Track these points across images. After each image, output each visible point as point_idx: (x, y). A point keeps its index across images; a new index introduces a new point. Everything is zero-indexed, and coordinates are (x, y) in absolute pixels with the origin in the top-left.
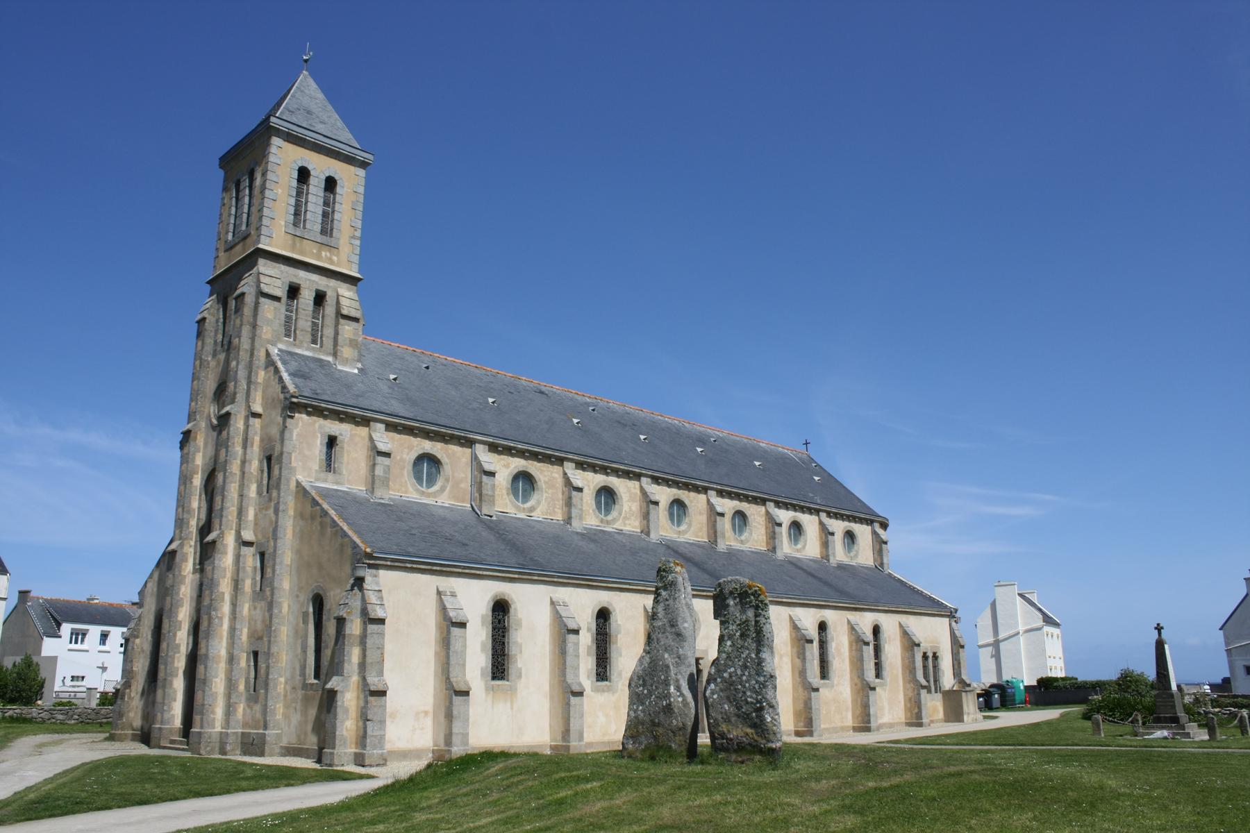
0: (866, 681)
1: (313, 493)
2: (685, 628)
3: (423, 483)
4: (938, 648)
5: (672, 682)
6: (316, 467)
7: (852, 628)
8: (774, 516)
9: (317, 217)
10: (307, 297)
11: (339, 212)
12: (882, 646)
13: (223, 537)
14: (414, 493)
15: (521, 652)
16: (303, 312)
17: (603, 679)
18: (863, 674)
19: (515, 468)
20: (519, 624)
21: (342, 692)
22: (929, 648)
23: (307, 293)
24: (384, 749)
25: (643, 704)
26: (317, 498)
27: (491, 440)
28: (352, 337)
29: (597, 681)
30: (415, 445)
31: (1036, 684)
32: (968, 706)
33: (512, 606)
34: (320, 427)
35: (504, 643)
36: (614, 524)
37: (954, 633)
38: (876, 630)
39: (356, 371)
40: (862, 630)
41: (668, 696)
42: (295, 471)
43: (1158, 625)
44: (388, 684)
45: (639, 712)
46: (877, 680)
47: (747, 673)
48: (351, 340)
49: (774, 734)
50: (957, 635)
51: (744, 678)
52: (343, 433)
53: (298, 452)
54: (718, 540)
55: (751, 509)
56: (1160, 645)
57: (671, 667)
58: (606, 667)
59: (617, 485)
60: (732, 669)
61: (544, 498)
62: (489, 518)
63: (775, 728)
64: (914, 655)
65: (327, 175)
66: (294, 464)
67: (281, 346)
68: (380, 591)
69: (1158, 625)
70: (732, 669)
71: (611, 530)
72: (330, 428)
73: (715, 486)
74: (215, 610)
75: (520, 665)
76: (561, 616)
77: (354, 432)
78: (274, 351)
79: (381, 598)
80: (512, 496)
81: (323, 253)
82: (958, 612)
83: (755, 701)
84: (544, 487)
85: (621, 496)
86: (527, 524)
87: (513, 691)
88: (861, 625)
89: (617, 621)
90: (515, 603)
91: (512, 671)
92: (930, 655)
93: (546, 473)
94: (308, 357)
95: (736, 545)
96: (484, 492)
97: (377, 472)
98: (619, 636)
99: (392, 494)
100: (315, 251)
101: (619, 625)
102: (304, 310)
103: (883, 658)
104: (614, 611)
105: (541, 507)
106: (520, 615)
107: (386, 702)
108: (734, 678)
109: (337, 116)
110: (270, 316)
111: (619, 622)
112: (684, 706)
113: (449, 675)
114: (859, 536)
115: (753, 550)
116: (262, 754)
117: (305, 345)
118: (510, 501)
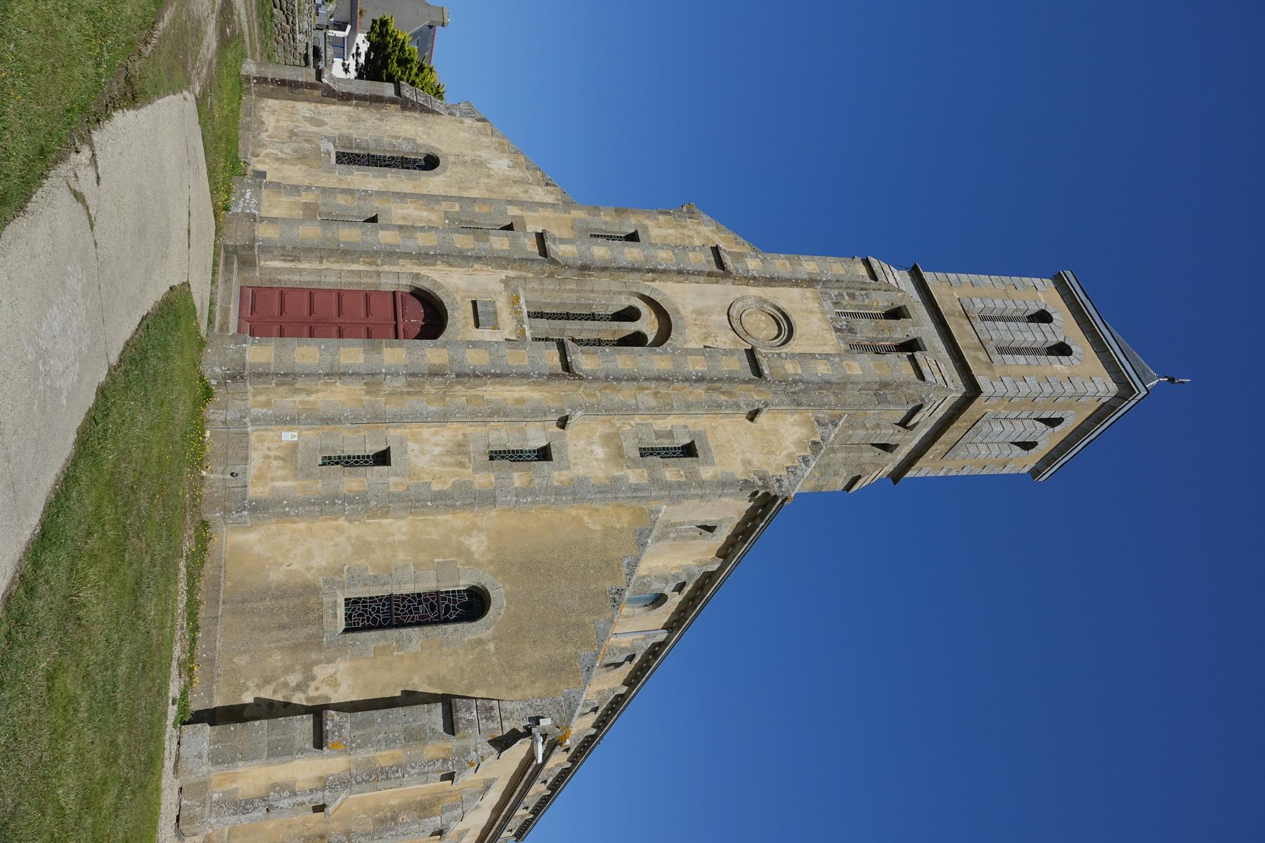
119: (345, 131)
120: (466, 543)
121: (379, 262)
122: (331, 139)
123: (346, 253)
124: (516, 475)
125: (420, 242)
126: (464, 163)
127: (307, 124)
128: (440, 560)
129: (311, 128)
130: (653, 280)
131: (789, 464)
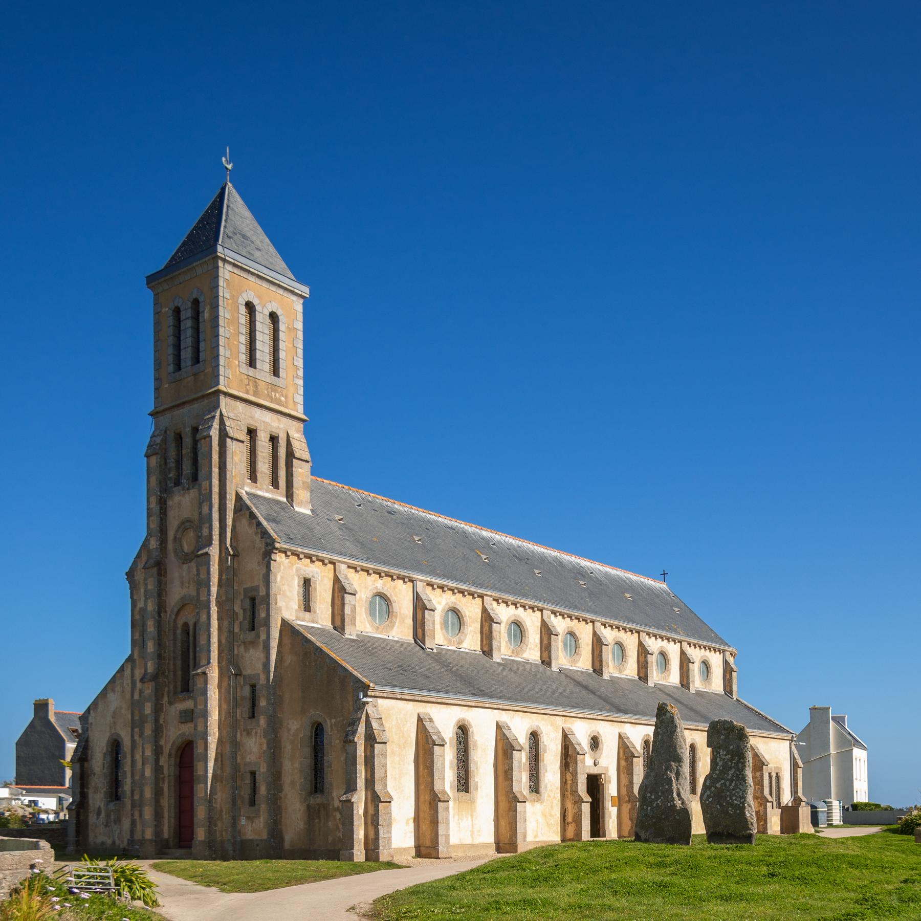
4: (779, 768)
6: (296, 606)
7: (622, 740)
9: (266, 356)
16: (261, 454)
20: (476, 745)
27: (429, 579)
33: (470, 730)
34: (298, 570)
39: (309, 513)
42: (281, 610)
47: (733, 784)
51: (731, 787)
52: (315, 575)
54: (603, 669)
60: (723, 781)
65: (270, 311)
67: (247, 489)
68: (381, 718)
71: (519, 659)
72: (305, 571)
89: (543, 742)
92: (774, 775)
101: (546, 745)
102: (262, 452)
106: (476, 738)
109: (269, 242)
115: (629, 677)
116: (599, 837)
117: (265, 487)
119: (102, 796)
120: (293, 731)
121: (162, 776)
122: (107, 804)
123: (158, 793)
124: (261, 704)
125: (149, 754)
126: (115, 723)
127: (101, 817)
128: (299, 745)
129: (103, 815)
130: (166, 612)
131: (259, 536)
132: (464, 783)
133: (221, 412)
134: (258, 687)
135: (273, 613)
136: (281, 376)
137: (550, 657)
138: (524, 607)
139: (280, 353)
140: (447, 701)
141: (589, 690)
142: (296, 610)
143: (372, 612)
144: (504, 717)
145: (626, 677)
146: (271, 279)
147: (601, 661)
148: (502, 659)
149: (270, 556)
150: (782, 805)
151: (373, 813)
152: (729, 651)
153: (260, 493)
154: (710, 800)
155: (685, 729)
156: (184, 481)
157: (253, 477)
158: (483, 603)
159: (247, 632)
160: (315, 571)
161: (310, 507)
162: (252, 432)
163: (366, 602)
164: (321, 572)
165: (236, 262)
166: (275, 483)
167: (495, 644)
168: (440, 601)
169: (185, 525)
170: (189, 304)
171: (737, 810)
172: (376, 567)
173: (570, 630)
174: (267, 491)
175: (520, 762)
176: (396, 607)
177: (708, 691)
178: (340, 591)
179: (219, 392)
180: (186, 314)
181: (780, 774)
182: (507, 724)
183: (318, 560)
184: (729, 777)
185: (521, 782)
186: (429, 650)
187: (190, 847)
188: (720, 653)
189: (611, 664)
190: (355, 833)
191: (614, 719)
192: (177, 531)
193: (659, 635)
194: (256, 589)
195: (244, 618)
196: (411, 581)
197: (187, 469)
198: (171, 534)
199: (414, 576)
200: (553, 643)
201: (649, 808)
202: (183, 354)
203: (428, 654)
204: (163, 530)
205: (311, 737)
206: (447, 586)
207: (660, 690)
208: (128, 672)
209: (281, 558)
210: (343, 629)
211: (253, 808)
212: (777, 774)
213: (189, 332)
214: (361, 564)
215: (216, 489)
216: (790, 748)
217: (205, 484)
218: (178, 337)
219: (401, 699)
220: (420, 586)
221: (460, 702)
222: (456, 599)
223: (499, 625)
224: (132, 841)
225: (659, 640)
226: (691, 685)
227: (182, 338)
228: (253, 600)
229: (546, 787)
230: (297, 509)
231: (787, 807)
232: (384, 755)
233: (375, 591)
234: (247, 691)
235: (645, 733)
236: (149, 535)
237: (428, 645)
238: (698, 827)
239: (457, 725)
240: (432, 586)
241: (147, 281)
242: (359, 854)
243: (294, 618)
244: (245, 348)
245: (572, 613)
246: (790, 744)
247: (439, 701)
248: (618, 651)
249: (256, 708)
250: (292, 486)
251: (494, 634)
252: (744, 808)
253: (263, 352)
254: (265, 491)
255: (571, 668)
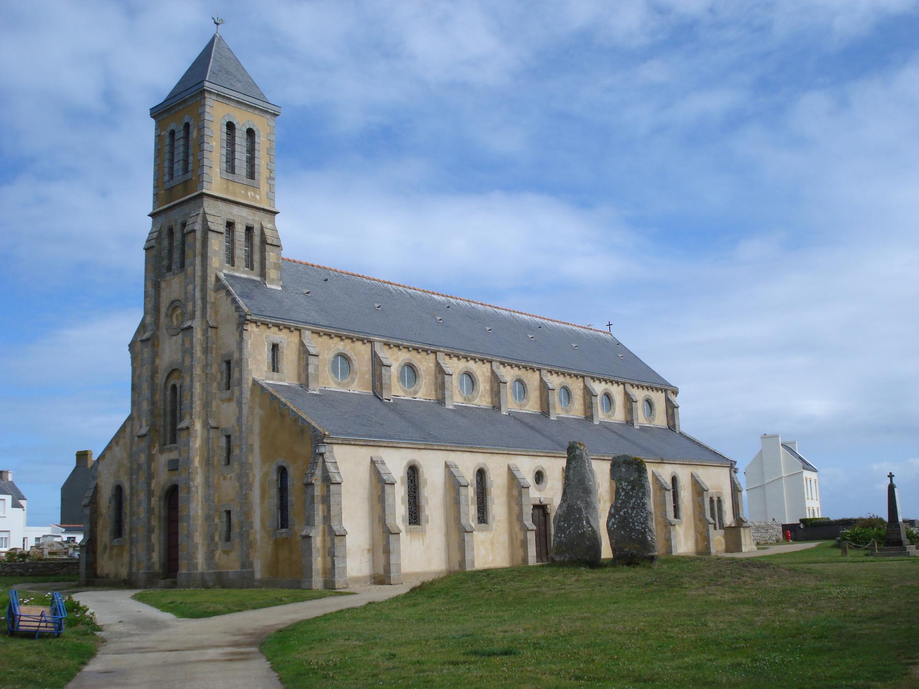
0: (668, 519)
1: (270, 389)
2: (590, 485)
3: (338, 376)
4: (721, 493)
5: (584, 519)
6: (265, 368)
8: (591, 390)
10: (240, 230)
11: (259, 158)
12: (679, 493)
13: (194, 424)
14: (334, 384)
15: (427, 503)
17: (481, 522)
18: (666, 515)
19: (402, 360)
20: (426, 483)
21: (315, 537)
22: (715, 494)
23: (240, 227)
24: (346, 577)
25: (565, 533)
26: (275, 394)
27: (386, 340)
28: (275, 261)
29: (479, 523)
30: (332, 347)
31: (674, 554)
32: (745, 539)
33: (421, 470)
35: (415, 497)
36: (473, 401)
37: (734, 481)
38: (674, 480)
39: (280, 288)
40: (665, 480)
41: (583, 527)
43: (890, 473)
44: (347, 530)
45: (563, 538)
46: (676, 520)
47: (635, 512)
48: (275, 264)
49: (653, 547)
50: (736, 483)
51: (633, 515)
52: (283, 341)
53: (252, 357)
54: (550, 411)
55: (574, 385)
56: (891, 488)
57: (583, 510)
58: (483, 512)
59: (475, 370)
60: (626, 510)
61: (424, 382)
62: (388, 401)
63: (653, 544)
64: (704, 499)
65: (248, 127)
66: (250, 367)
67: (225, 271)
69: (890, 473)
70: (626, 510)
73: (546, 368)
74: (193, 480)
75: (427, 513)
76: (454, 475)
77: (290, 340)
78: (222, 276)
79: (337, 468)
80: (401, 383)
81: (249, 193)
82: (737, 464)
83: (641, 528)
84: (423, 374)
85: (478, 378)
86: (414, 403)
87: (424, 532)
88: (663, 477)
89: (490, 478)
90: (422, 467)
91: (423, 518)
92: (715, 499)
93: (424, 363)
94: (245, 279)
95: (563, 415)
96: (384, 382)
97: (310, 371)
98: (492, 489)
99: (321, 387)
100: (243, 192)
101: (492, 481)
102: (239, 241)
103: (680, 502)
104: (488, 470)
105: (422, 390)
106: (426, 477)
107: (346, 543)
108: (627, 515)
110: (216, 248)
111: (492, 479)
112: (593, 533)
113: (385, 522)
114: (655, 402)
117: (242, 269)
118: (400, 386)
132: (415, 516)
133: (204, 209)
134: (232, 438)
135: (245, 375)
136: (256, 178)
137: (499, 402)
138: (519, 367)
139: (256, 160)
140: (398, 445)
141: (535, 430)
142: (266, 371)
143: (334, 370)
144: (454, 458)
145: (573, 417)
146: (248, 103)
147: (548, 404)
148: (454, 405)
149: (243, 326)
150: (725, 526)
151: (330, 546)
152: (671, 390)
153: (237, 274)
154: (615, 526)
155: (592, 459)
156: (174, 267)
157: (231, 260)
158: (436, 359)
159: (224, 391)
160: (282, 337)
161: (281, 283)
162: (230, 225)
163: (329, 361)
164: (288, 338)
165: (219, 93)
166: (250, 265)
167: (447, 393)
168: (395, 359)
169: (174, 305)
170: (182, 127)
171: (639, 535)
172: (337, 332)
173: (518, 378)
174: (244, 272)
175: (467, 496)
176: (356, 364)
177: (652, 426)
178: (304, 353)
179: (203, 195)
180: (180, 134)
181: (722, 498)
182: (455, 463)
183: (285, 327)
184: (631, 506)
185: (468, 514)
186: (386, 401)
187: (175, 577)
188: (662, 392)
189: (558, 405)
190: (314, 564)
191: (557, 455)
192: (168, 309)
193: (602, 378)
194: (232, 355)
195: (222, 379)
196: (370, 342)
197: (176, 255)
198: (163, 310)
199: (372, 338)
200: (502, 390)
201: (563, 536)
202: (176, 166)
203: (386, 404)
204: (157, 309)
205: (277, 480)
206: (402, 345)
207: (605, 427)
208: (128, 429)
209: (252, 327)
210: (307, 386)
211: (228, 543)
212: (718, 498)
213: (181, 149)
214: (324, 330)
215: (199, 273)
216: (730, 474)
217: (189, 270)
218: (172, 153)
219: (354, 445)
220: (378, 347)
221: (410, 446)
222: (411, 355)
223: (450, 377)
224: (130, 573)
225: (603, 383)
226: (635, 422)
227: (175, 154)
228: (228, 363)
229: (494, 518)
230: (268, 286)
231: (730, 527)
232: (340, 494)
233: (337, 352)
234: (223, 442)
235: (76, 453)
236: (146, 313)
237: (385, 396)
238: (606, 552)
239: (408, 466)
240: (389, 345)
241: (151, 112)
242: (317, 581)
243: (264, 378)
244: (225, 158)
245: (520, 363)
246: (730, 471)
247: (390, 445)
248: (605, 401)
249: (230, 456)
250: (265, 268)
251: (447, 385)
252: (645, 532)
253: (241, 160)
254: (242, 273)
255: (520, 411)
